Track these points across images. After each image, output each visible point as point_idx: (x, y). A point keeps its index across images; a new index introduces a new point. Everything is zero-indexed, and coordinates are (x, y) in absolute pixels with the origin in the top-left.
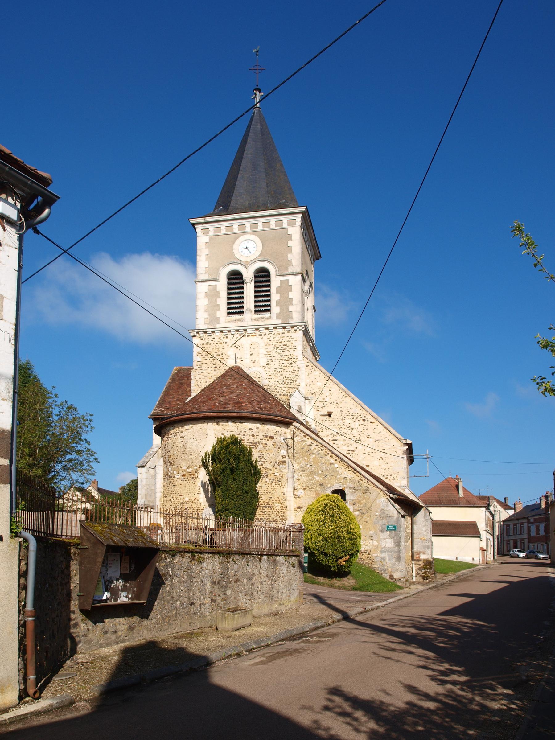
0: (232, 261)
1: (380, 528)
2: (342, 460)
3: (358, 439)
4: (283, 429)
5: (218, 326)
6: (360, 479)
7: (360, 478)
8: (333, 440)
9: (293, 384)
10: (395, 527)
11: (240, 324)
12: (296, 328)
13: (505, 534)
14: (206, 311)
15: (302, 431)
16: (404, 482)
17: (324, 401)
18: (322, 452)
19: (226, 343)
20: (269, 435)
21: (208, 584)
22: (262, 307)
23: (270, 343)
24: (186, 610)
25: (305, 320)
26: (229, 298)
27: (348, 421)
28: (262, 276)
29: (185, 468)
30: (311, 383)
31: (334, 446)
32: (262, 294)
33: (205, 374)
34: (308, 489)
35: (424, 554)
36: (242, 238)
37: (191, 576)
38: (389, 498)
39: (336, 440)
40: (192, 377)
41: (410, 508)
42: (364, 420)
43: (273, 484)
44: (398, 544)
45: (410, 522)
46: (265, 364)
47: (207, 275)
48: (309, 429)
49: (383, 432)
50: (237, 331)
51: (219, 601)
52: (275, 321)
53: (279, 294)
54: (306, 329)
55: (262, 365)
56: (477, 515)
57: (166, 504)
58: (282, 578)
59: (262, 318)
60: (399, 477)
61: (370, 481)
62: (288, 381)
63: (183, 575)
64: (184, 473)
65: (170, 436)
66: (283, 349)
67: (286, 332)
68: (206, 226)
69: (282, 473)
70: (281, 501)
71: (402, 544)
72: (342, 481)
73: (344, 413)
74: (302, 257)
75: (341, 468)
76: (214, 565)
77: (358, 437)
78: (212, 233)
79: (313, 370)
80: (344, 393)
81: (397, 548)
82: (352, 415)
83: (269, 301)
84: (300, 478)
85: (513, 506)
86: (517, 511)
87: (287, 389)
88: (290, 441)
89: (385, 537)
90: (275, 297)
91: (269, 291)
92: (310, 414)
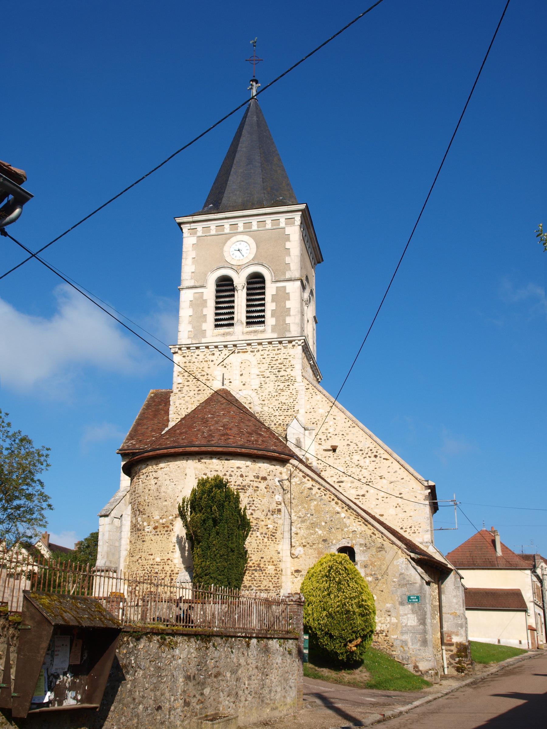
0: (221, 265)
1: (400, 600)
3: (369, 480)
6: (373, 533)
7: (372, 531)
11: (228, 338)
12: (294, 343)
15: (300, 470)
16: (427, 537)
19: (212, 361)
20: (261, 476)
22: (255, 318)
23: (264, 361)
28: (256, 282)
30: (312, 410)
34: (308, 546)
35: (457, 635)
36: (234, 239)
37: (159, 667)
39: (342, 482)
42: (376, 456)
43: (266, 540)
44: (423, 621)
51: (195, 704)
53: (274, 304)
56: (520, 581)
59: (255, 332)
61: (385, 535)
65: (141, 477)
67: (282, 348)
68: (193, 226)
69: (276, 525)
70: (275, 563)
78: (200, 233)
79: (314, 394)
80: (351, 422)
81: (421, 627)
82: (361, 450)
83: (263, 311)
84: (299, 531)
87: (283, 417)
88: (286, 483)
89: (406, 612)
90: (270, 306)
91: (263, 299)
92: (311, 449)
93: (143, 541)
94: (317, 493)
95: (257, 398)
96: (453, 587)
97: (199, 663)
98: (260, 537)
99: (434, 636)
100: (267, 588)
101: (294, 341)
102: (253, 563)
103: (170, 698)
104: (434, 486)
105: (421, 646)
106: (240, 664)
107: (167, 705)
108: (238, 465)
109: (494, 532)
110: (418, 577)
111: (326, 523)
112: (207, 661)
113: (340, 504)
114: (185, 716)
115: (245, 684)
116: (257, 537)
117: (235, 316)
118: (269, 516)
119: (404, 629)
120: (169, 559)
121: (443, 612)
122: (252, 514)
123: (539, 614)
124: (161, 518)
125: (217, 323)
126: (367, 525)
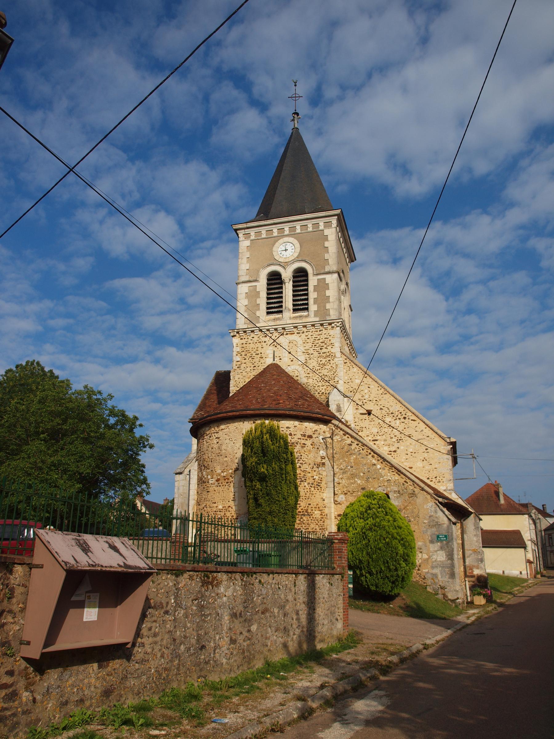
0: (271, 262)
1: (430, 538)
3: (399, 438)
4: (323, 427)
6: (405, 482)
7: (404, 480)
8: (373, 441)
10: (446, 536)
11: (278, 322)
12: (333, 325)
13: (547, 545)
15: (341, 429)
16: (451, 486)
17: (363, 398)
18: (363, 452)
19: (265, 342)
20: (307, 434)
21: (226, 618)
22: (301, 305)
23: (308, 341)
26: (268, 298)
28: (301, 276)
30: (349, 381)
32: (299, 288)
33: (244, 374)
34: (349, 494)
35: (478, 568)
36: (281, 241)
37: (203, 606)
38: (437, 502)
39: (376, 440)
41: (459, 512)
42: (405, 418)
43: (313, 489)
44: (450, 556)
45: (460, 531)
47: (248, 276)
49: (425, 431)
50: (276, 329)
51: (241, 641)
53: (316, 293)
56: (521, 524)
59: (300, 317)
60: (444, 479)
61: (416, 483)
63: (191, 606)
65: (206, 437)
66: (321, 347)
67: (324, 329)
68: (247, 231)
69: (321, 476)
70: (321, 508)
72: (386, 484)
76: (235, 590)
78: (253, 237)
79: (351, 367)
80: (383, 390)
81: (449, 562)
82: (392, 413)
83: (307, 299)
84: (340, 481)
87: (325, 387)
88: (329, 440)
89: (436, 549)
90: (312, 295)
91: (307, 290)
92: (349, 413)
93: (208, 492)
94: (356, 448)
95: (302, 372)
96: (473, 528)
97: (245, 600)
98: (307, 487)
99: (459, 570)
100: (314, 530)
101: (334, 323)
102: (302, 509)
103: (215, 637)
104: (455, 442)
105: (449, 578)
106: (287, 600)
107: (212, 644)
108: (287, 426)
109: (498, 485)
110: (446, 519)
111: (364, 474)
112: (253, 598)
113: (376, 458)
114: (232, 654)
115: (293, 619)
116: (305, 486)
117: (284, 304)
118: (315, 469)
119: (434, 564)
120: (230, 507)
121: (466, 549)
122: (300, 467)
123: (535, 550)
124: (222, 472)
125: (268, 306)
126: (399, 475)
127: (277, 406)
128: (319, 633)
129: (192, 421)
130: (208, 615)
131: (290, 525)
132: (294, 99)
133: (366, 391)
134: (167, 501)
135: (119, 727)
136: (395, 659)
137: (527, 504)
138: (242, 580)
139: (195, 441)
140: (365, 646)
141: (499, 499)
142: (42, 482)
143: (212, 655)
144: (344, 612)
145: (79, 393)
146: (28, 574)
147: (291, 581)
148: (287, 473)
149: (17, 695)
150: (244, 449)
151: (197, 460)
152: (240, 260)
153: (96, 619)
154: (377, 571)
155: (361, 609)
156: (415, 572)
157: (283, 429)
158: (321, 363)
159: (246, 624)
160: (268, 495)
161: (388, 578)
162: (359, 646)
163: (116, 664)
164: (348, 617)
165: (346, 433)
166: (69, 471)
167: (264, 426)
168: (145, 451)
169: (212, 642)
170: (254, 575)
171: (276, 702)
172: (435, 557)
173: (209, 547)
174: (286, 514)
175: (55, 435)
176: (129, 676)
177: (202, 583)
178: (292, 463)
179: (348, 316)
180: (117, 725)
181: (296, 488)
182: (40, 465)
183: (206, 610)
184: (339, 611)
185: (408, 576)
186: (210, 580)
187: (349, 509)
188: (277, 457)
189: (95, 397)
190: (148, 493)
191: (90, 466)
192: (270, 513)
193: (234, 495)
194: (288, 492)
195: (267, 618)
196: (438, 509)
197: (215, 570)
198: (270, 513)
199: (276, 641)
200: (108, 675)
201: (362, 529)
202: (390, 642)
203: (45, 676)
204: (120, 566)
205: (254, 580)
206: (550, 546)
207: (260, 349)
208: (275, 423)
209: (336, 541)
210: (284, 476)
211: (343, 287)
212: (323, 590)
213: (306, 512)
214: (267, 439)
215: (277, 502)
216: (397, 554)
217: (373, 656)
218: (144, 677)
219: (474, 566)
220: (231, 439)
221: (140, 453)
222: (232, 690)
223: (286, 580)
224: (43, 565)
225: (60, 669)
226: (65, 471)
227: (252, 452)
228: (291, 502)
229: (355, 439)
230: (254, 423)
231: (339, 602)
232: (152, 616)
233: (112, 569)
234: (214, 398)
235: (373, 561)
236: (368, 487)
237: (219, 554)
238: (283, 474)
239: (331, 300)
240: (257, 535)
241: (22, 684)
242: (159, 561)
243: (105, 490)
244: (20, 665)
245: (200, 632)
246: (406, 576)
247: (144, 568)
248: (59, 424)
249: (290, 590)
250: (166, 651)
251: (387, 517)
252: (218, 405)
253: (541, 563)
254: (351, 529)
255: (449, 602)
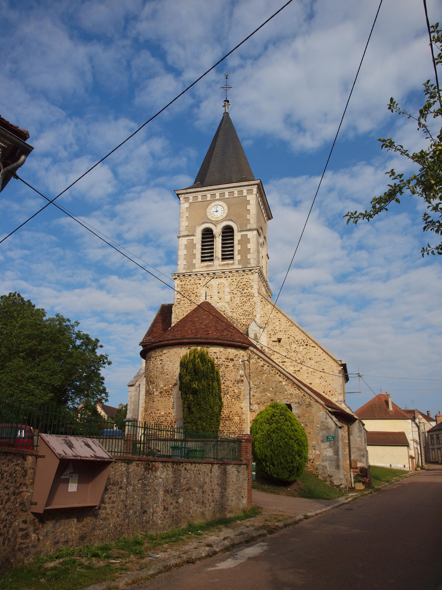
0: (205, 221)
1: (321, 439)
2: (288, 378)
3: (302, 361)
4: (242, 352)
5: (194, 270)
6: (304, 395)
7: (303, 394)
8: (282, 362)
9: (250, 316)
10: (333, 437)
11: (210, 269)
12: (252, 271)
13: (430, 443)
14: (185, 259)
15: (256, 354)
19: (199, 284)
20: (230, 358)
21: (161, 493)
22: (228, 255)
23: (233, 283)
24: (138, 519)
25: (261, 265)
26: (202, 249)
27: (294, 346)
28: (228, 232)
29: (162, 386)
30: (265, 315)
31: (283, 367)
32: (227, 242)
33: (183, 308)
34: (261, 404)
35: (360, 462)
36: (213, 204)
37: (145, 484)
38: (327, 411)
39: (285, 362)
40: (173, 311)
42: (307, 345)
43: (233, 400)
44: (336, 453)
45: (347, 433)
46: (229, 300)
47: (187, 232)
48: (263, 353)
49: (322, 355)
50: (208, 274)
51: (172, 509)
52: (237, 266)
54: (260, 272)
55: (227, 301)
57: (146, 417)
58: (231, 486)
59: (227, 264)
60: (336, 393)
61: (312, 396)
62: (246, 313)
63: (137, 484)
64: (162, 390)
65: (152, 359)
67: (245, 275)
68: (187, 196)
69: (240, 390)
71: (340, 453)
73: (290, 340)
74: (257, 217)
75: (288, 385)
76: (167, 474)
77: (302, 359)
78: (191, 201)
79: (266, 304)
80: (290, 323)
81: (335, 456)
82: (297, 341)
83: (233, 251)
84: (255, 394)
85: (434, 419)
86: (438, 423)
87: (246, 320)
88: (247, 362)
89: (326, 447)
90: (237, 247)
91: (233, 243)
92: (264, 341)
93: (153, 401)
95: (228, 308)
96: (358, 431)
97: (175, 481)
100: (234, 431)
101: (253, 270)
105: (335, 469)
107: (151, 510)
108: (215, 351)
109: (388, 395)
112: (180, 480)
113: (282, 376)
114: (165, 517)
115: (209, 495)
116: (228, 398)
117: (214, 254)
122: (224, 383)
123: (417, 448)
125: (203, 255)
126: (299, 390)
127: (207, 336)
128: (228, 506)
129: (142, 344)
130: (148, 491)
131: (215, 428)
132: (228, 86)
133: (277, 323)
134: (121, 406)
135: (90, 558)
136: (281, 524)
137: (414, 411)
138: (173, 467)
139: (144, 361)
140: (262, 516)
141: (388, 407)
142: (22, 391)
143: (151, 518)
144: (248, 492)
145: (52, 320)
146: (35, 461)
147: (208, 469)
148: (213, 388)
149: (29, 535)
150: (181, 369)
151: (145, 377)
152: (181, 219)
153: (76, 491)
154: (278, 463)
155: (266, 492)
156: (309, 465)
157: (211, 354)
158: (243, 301)
159: (175, 497)
160: (198, 405)
161: (286, 469)
162: (258, 516)
163: (88, 520)
164: (251, 496)
165: (259, 357)
166: (44, 383)
167: (196, 351)
168: (104, 367)
169: (151, 508)
170: (181, 464)
171: (192, 547)
172: (325, 453)
173: (152, 445)
174: (212, 419)
175: (32, 354)
176: (96, 528)
177: (145, 469)
178: (217, 381)
179: (265, 263)
180: (89, 556)
181: (220, 399)
182: (20, 378)
183: (147, 487)
184: (245, 491)
185: (302, 467)
186: (151, 467)
187: (259, 416)
188: (205, 376)
189: (65, 324)
190: (106, 400)
191: (60, 379)
192: (200, 418)
193: (173, 404)
194: (214, 403)
195: (190, 494)
196: (328, 416)
197: (154, 460)
198: (200, 418)
199: (196, 510)
200: (83, 526)
201: (268, 432)
202: (281, 513)
203: (45, 525)
204: (92, 457)
205: (182, 468)
206: (432, 444)
207: (195, 289)
208: (205, 349)
209: (244, 441)
210: (211, 390)
211: (261, 240)
212: (232, 476)
213: (228, 417)
214: (198, 362)
215: (205, 410)
216: (293, 450)
217: (266, 522)
218: (106, 529)
219: (357, 460)
220: (172, 360)
221: (100, 368)
222: (163, 540)
223: (205, 468)
224: (45, 456)
225: (54, 521)
226: (40, 383)
227: (186, 372)
228: (216, 410)
229: (267, 361)
230: (189, 349)
231: (245, 485)
232: (112, 490)
233: (87, 459)
234: (160, 325)
235: (275, 455)
236: (276, 399)
237: (159, 449)
238: (210, 389)
239: (251, 251)
240: (189, 435)
241: (31, 529)
242: (116, 454)
243: (71, 397)
244: (30, 518)
245: (143, 502)
246: (300, 467)
247: (107, 458)
248: (35, 345)
249: (208, 475)
250: (120, 513)
251: (287, 422)
252: (162, 334)
253: (423, 458)
254: (259, 431)
255: (335, 487)
